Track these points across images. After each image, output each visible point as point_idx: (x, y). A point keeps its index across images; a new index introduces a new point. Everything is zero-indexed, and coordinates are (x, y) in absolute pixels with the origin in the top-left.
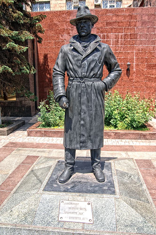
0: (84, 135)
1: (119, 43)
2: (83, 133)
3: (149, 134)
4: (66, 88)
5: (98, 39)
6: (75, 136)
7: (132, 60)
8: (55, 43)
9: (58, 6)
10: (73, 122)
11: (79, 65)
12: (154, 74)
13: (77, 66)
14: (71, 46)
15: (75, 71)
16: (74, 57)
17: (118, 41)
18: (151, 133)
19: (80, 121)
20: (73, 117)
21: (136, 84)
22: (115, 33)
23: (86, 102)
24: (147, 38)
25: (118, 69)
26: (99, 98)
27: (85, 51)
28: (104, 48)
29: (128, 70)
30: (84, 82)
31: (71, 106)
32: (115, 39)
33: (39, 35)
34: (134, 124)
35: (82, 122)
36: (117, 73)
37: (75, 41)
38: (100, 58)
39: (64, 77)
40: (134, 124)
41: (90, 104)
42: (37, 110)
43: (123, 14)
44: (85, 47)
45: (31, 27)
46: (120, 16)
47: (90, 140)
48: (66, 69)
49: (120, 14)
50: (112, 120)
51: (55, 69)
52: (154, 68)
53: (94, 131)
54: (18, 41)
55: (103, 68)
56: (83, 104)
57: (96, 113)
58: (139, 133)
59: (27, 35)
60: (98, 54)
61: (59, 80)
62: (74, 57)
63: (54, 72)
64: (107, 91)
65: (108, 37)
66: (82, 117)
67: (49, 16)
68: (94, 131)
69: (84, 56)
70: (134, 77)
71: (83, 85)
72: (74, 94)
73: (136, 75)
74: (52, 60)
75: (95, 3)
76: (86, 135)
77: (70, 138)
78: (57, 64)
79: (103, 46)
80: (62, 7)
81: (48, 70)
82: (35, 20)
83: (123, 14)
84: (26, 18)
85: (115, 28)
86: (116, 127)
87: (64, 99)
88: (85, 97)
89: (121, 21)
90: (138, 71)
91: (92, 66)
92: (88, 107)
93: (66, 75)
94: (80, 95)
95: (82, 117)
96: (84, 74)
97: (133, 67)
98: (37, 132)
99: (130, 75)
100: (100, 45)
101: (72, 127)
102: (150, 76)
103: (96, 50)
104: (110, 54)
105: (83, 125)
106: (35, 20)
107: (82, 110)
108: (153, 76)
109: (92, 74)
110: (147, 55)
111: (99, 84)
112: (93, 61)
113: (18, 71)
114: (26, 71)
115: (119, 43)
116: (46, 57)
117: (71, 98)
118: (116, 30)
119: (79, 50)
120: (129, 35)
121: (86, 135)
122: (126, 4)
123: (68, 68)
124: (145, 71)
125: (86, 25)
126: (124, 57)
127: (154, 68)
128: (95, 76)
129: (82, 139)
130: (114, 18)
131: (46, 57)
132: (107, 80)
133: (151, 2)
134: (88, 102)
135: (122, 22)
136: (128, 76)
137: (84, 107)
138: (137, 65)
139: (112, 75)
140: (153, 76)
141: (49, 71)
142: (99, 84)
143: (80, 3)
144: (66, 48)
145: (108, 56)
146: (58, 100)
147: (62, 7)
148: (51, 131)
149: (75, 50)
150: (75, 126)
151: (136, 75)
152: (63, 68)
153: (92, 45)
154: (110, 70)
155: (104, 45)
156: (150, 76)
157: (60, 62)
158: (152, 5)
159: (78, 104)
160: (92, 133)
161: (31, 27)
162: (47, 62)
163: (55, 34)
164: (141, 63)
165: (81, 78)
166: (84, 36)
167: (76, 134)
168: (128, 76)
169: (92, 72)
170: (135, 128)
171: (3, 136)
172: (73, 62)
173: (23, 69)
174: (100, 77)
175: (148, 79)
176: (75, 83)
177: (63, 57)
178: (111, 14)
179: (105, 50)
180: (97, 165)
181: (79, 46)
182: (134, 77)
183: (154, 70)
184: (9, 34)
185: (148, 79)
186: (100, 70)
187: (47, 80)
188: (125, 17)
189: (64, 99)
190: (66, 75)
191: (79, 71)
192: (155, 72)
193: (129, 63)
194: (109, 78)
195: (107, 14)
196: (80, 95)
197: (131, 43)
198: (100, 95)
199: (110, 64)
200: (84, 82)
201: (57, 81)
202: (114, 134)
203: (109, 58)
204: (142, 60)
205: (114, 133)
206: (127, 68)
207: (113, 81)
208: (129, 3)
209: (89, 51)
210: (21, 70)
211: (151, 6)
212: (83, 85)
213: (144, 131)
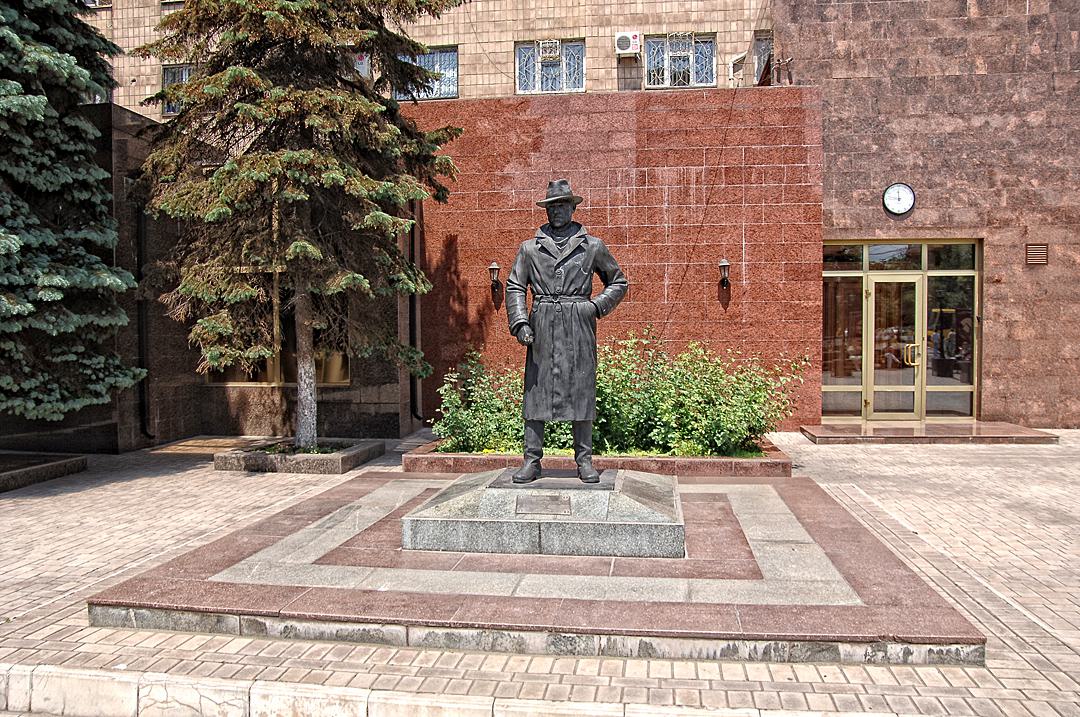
0: (559, 394)
1: (691, 197)
2: (558, 389)
3: (761, 464)
4: (529, 311)
5: (583, 231)
6: (544, 396)
7: (734, 252)
8: (481, 197)
9: (486, 61)
10: (541, 370)
11: (551, 274)
12: (812, 297)
13: (548, 275)
14: (537, 243)
15: (543, 284)
16: (543, 260)
17: (687, 193)
18: (766, 464)
19: (552, 369)
20: (541, 362)
21: (752, 331)
22: (678, 165)
23: (563, 335)
24: (781, 181)
25: (620, 280)
26: (585, 328)
27: (561, 251)
28: (593, 246)
29: (724, 283)
30: (559, 302)
31: (537, 341)
32: (679, 183)
33: (440, 179)
34: (718, 439)
35: (556, 370)
36: (618, 288)
37: (544, 235)
38: (585, 263)
39: (526, 293)
40: (718, 439)
41: (569, 340)
42: (415, 419)
43: (700, 105)
44: (561, 245)
45: (419, 163)
46: (692, 113)
47: (571, 402)
48: (529, 281)
49: (689, 106)
50: (655, 431)
51: (511, 281)
52: (811, 275)
53: (576, 387)
54: (388, 204)
55: (591, 279)
56: (558, 339)
57: (580, 355)
58: (731, 463)
59: (411, 186)
60: (581, 256)
61: (518, 298)
62: (543, 260)
63: (508, 285)
64: (599, 318)
65: (653, 178)
66: (556, 361)
67: (462, 115)
68: (576, 387)
69: (559, 260)
70: (745, 309)
71: (558, 307)
72: (543, 322)
73: (750, 300)
74: (470, 253)
75: (618, 51)
76: (563, 394)
77: (534, 400)
78: (515, 272)
79: (591, 243)
80: (500, 63)
81: (458, 288)
82: (432, 142)
83: (700, 105)
84: (408, 141)
85: (676, 152)
86: (665, 448)
87: (525, 328)
88: (562, 328)
89: (696, 128)
90: (757, 290)
91: (572, 275)
92: (565, 343)
93: (529, 291)
94: (552, 325)
95: (556, 361)
96: (558, 288)
97: (739, 274)
98: (432, 463)
99: (730, 302)
100: (586, 242)
101: (538, 380)
102: (798, 302)
103: (579, 249)
104: (604, 254)
105: (557, 375)
106: (432, 142)
107: (556, 350)
108: (811, 303)
109: (572, 289)
110: (787, 236)
111: (585, 305)
112: (574, 267)
113: (383, 285)
114: (407, 284)
115: (692, 199)
116: (451, 243)
117: (537, 329)
118: (683, 157)
119: (550, 250)
120: (723, 170)
121: (563, 394)
122: (731, 53)
123: (532, 279)
124: (781, 286)
125: (562, 211)
126: (710, 242)
127: (810, 276)
128: (577, 292)
129: (557, 400)
130: (672, 121)
131: (451, 243)
132: (599, 299)
133: (793, 68)
134: (567, 335)
135: (698, 132)
136: (725, 306)
137: (558, 344)
138: (754, 268)
139: (609, 290)
140: (811, 303)
141: (459, 293)
142: (585, 305)
143: (564, 51)
144: (530, 246)
145: (599, 259)
146: (515, 330)
147: (500, 63)
148: (473, 459)
149: (543, 249)
150: (543, 379)
151: (750, 300)
152: (525, 280)
153: (573, 241)
154: (607, 281)
155: (594, 241)
156: (798, 302)
157: (518, 269)
158: (794, 79)
159: (549, 340)
160: (572, 390)
161: (419, 163)
162: (454, 261)
163: (479, 171)
164: (766, 261)
165: (555, 296)
166: (558, 228)
167: (546, 393)
168: (725, 306)
169: (573, 285)
170: (721, 452)
171: (331, 476)
172: (541, 270)
173: (399, 280)
174: (587, 294)
175: (791, 314)
176: (544, 304)
177: (524, 262)
178: (662, 108)
179: (595, 249)
180: (585, 455)
181: (549, 241)
182: (743, 306)
183: (812, 283)
184: (369, 191)
185: (791, 314)
186: (587, 282)
187: (451, 320)
188: (706, 115)
189: (525, 328)
190: (529, 291)
191: (551, 284)
192: (813, 288)
193: (725, 262)
194: (603, 296)
195: (651, 108)
196: (552, 325)
197: (731, 198)
198: (586, 324)
199: (605, 272)
200: (559, 302)
201: (515, 300)
202: (659, 465)
203: (602, 262)
204: (770, 251)
205: (657, 462)
206: (719, 279)
207: (612, 302)
208: (740, 50)
209: (568, 252)
210: (392, 282)
211: (791, 83)
212: (558, 307)
213: (744, 457)
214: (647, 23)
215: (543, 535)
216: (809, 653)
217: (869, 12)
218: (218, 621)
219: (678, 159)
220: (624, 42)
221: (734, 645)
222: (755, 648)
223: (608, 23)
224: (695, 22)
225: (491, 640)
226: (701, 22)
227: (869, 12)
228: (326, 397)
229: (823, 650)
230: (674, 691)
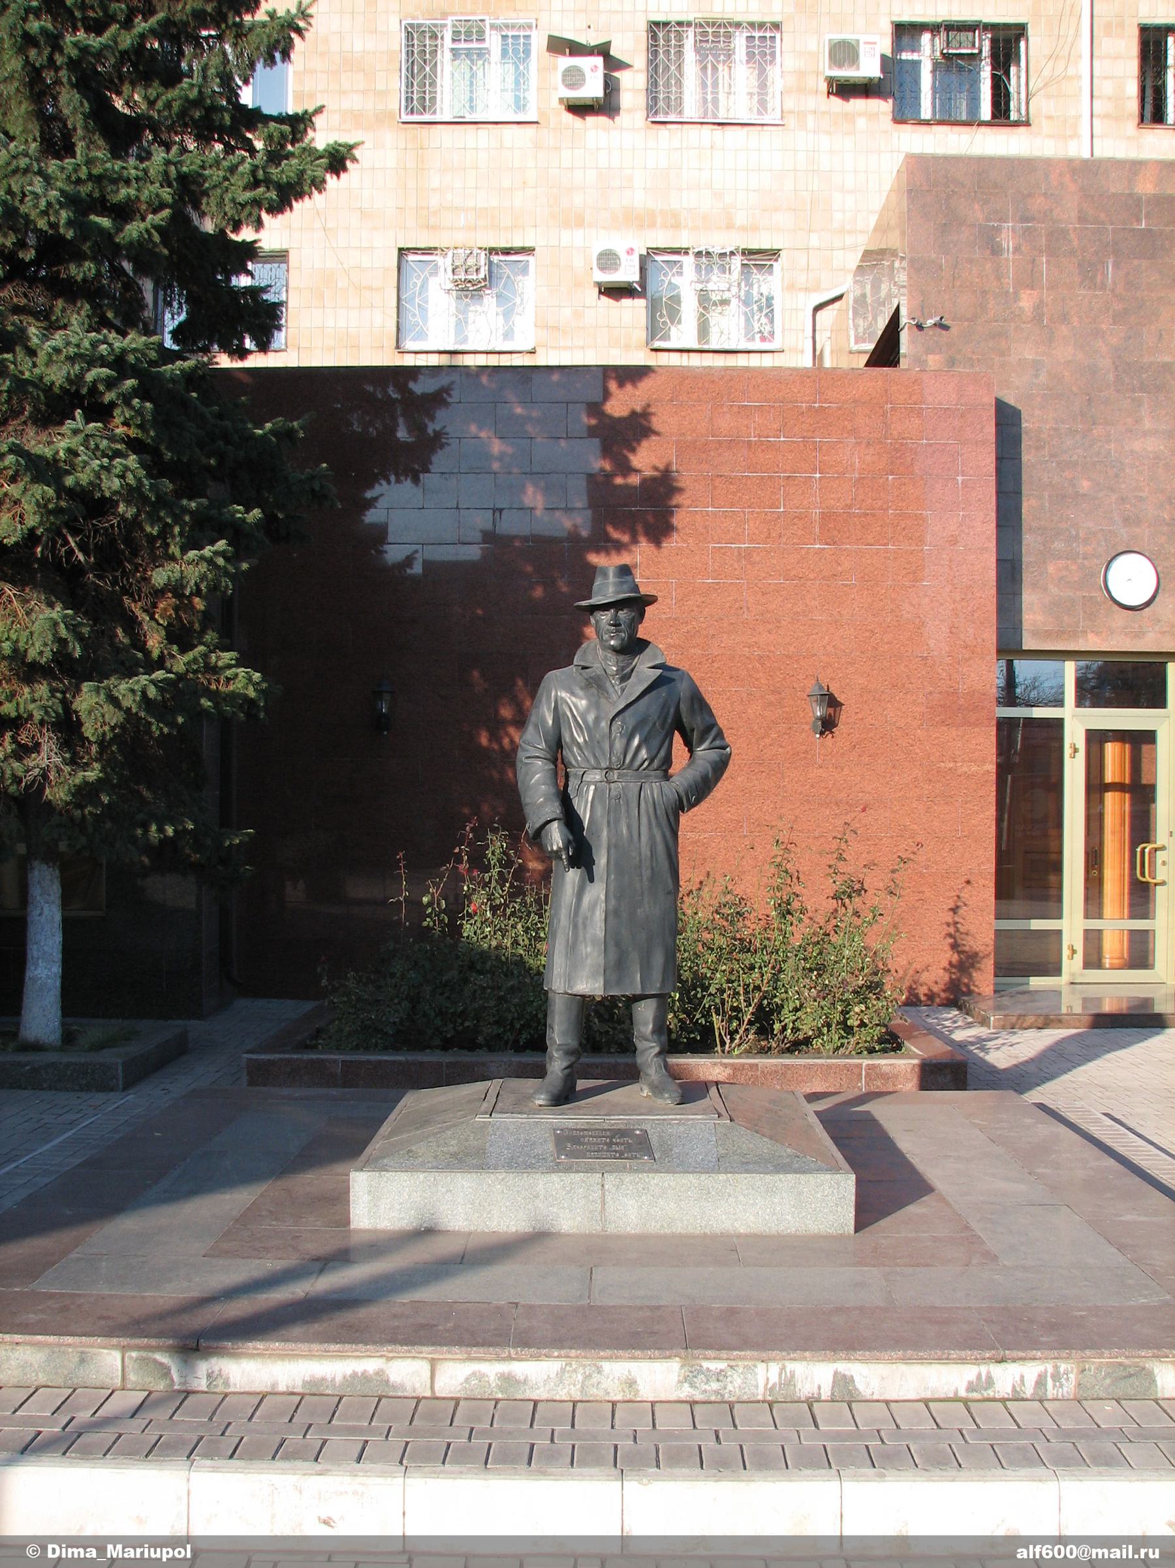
80: (371, 289)
102: (951, 765)
108: (974, 768)
147: (371, 289)
156: (951, 765)
214: (653, 225)
215: (608, 1198)
216: (1108, 1381)
217: (1076, 243)
218: (82, 1361)
219: (734, 494)
220: (608, 259)
221: (989, 1373)
222: (1022, 1377)
223: (580, 222)
224: (743, 229)
225: (580, 1377)
226: (754, 228)
227: (1076, 243)
228: (622, 1060)
229: (1131, 1375)
230: (552, 1440)
